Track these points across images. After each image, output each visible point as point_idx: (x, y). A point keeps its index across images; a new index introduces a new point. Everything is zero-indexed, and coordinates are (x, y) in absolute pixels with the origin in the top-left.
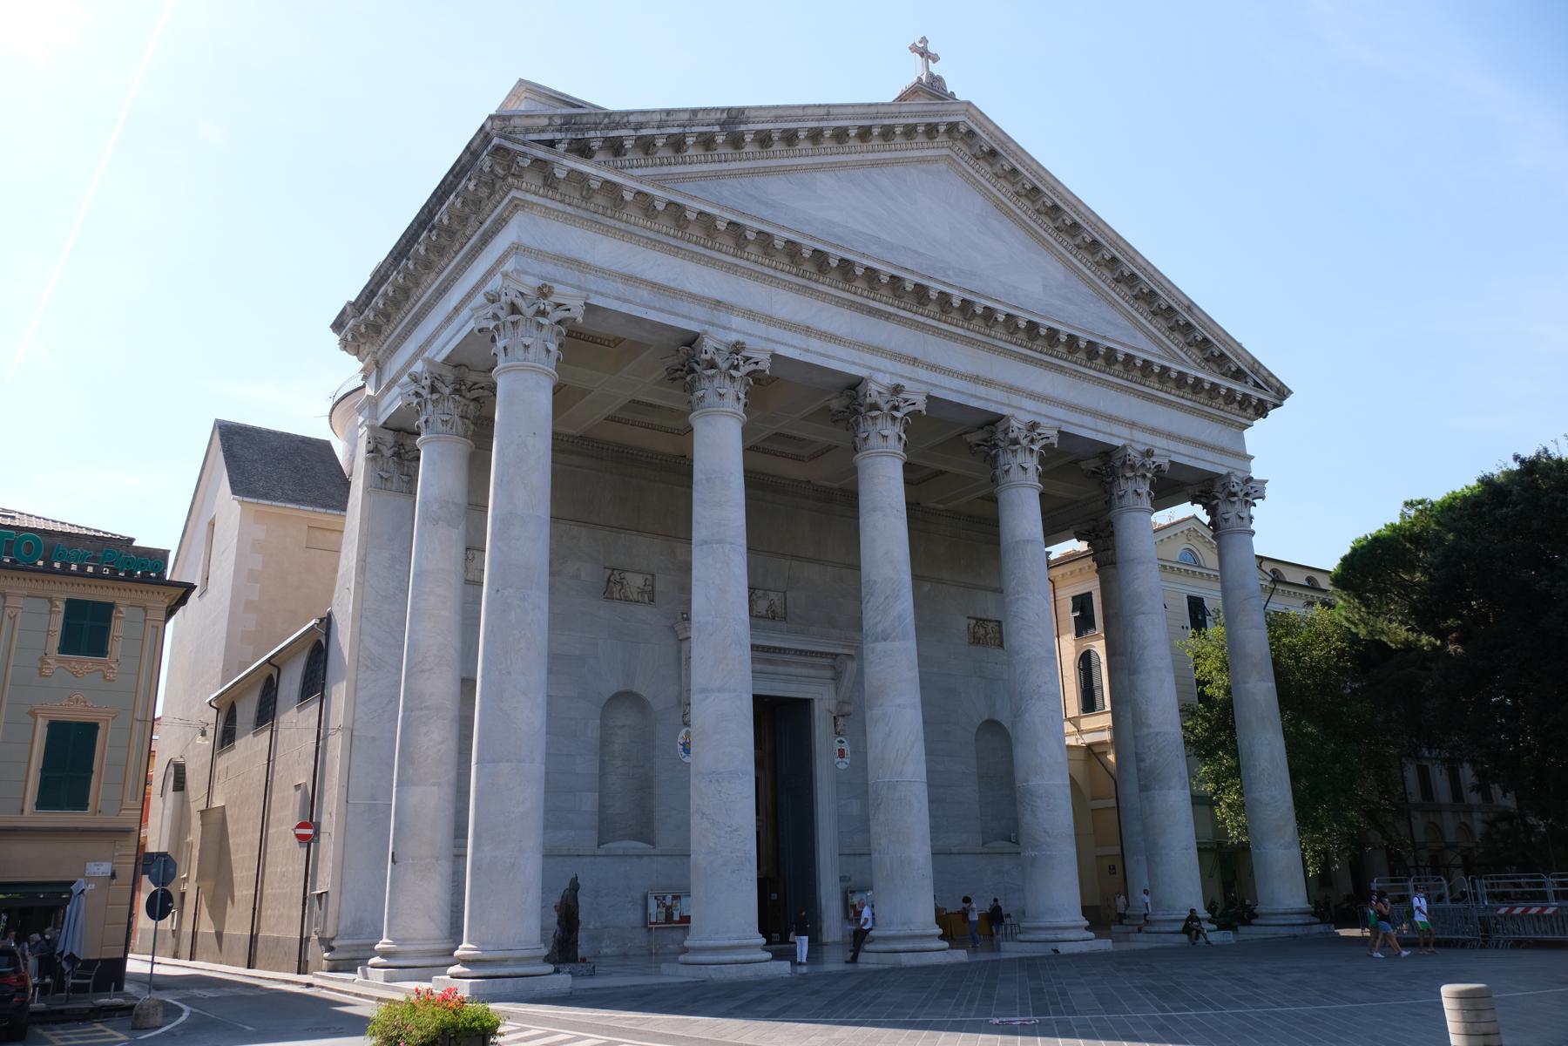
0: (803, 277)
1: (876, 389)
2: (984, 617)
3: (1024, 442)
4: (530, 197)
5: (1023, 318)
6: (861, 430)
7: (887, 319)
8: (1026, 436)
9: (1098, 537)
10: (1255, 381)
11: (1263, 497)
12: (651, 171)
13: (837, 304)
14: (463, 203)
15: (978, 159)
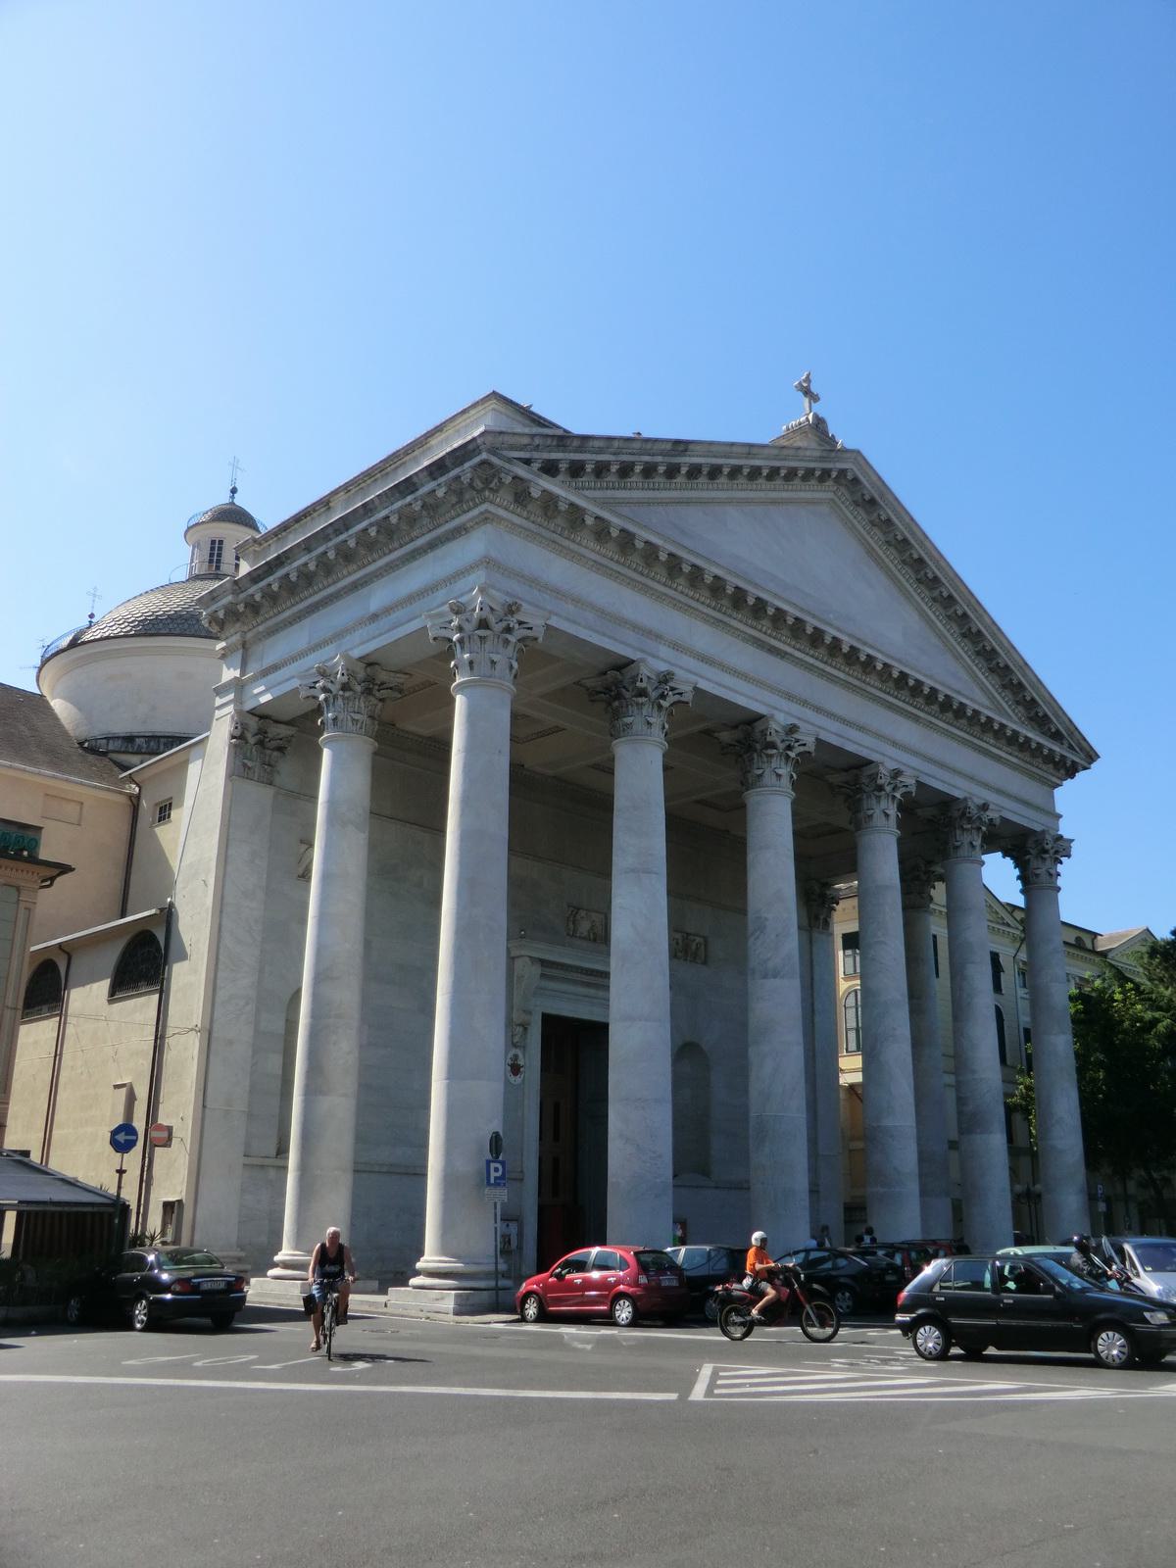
0: (719, 611)
3: (888, 789)
4: (501, 512)
5: (898, 667)
6: (755, 766)
7: (782, 658)
8: (890, 783)
10: (1070, 744)
11: (1069, 856)
12: (597, 494)
14: (422, 507)
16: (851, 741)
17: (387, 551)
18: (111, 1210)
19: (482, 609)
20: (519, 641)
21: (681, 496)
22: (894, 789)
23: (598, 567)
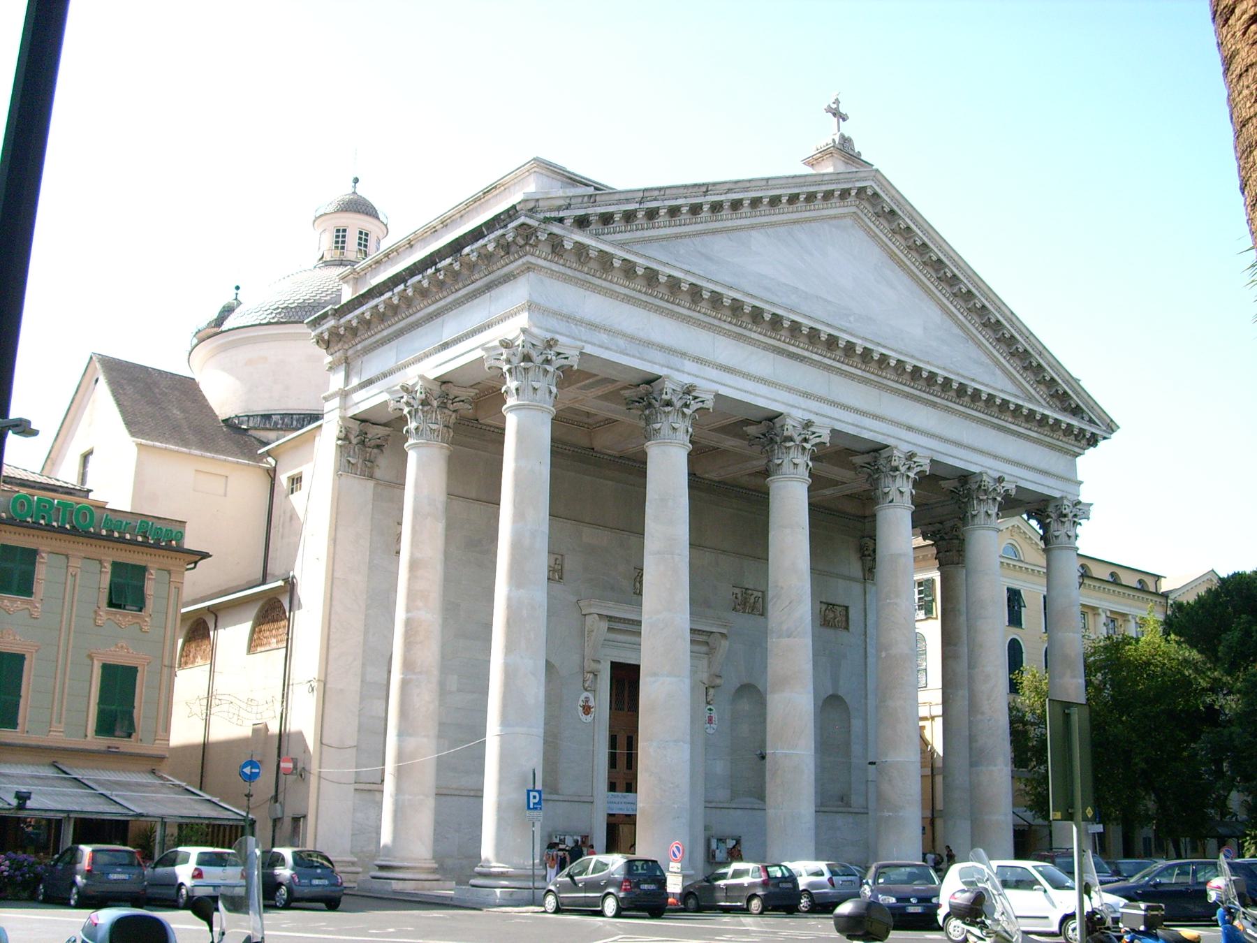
0: (740, 326)
1: (791, 427)
2: (833, 602)
3: (903, 469)
5: (910, 363)
7: (801, 361)
8: (904, 464)
9: (942, 538)
10: (1090, 418)
11: (1088, 519)
13: (764, 349)
15: (879, 216)
16: (865, 429)
17: (454, 290)
18: (242, 823)
19: (523, 347)
20: (557, 369)
21: (705, 228)
22: (909, 469)
23: (628, 299)
